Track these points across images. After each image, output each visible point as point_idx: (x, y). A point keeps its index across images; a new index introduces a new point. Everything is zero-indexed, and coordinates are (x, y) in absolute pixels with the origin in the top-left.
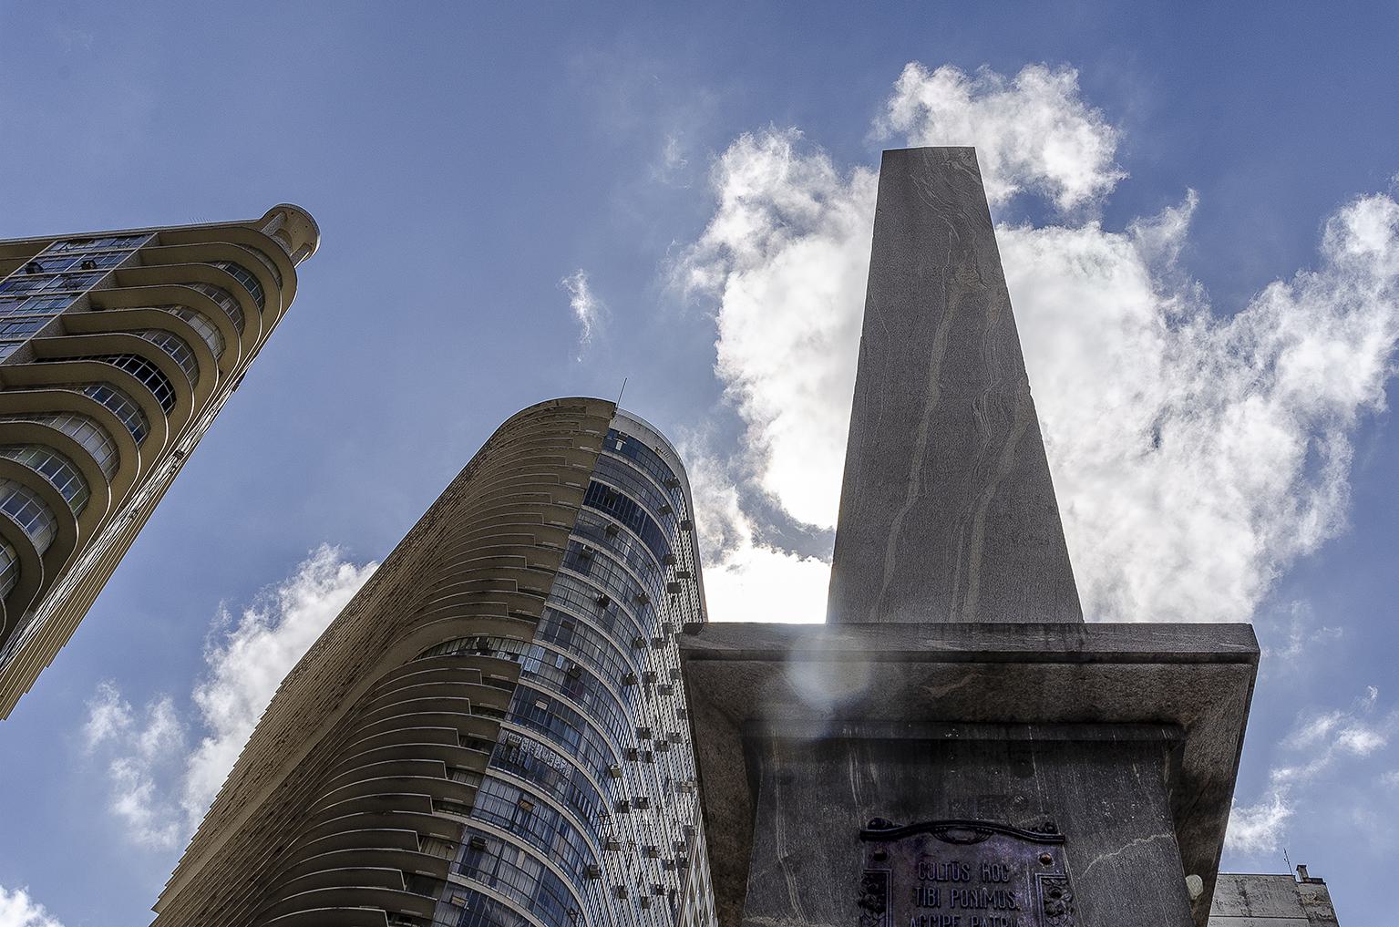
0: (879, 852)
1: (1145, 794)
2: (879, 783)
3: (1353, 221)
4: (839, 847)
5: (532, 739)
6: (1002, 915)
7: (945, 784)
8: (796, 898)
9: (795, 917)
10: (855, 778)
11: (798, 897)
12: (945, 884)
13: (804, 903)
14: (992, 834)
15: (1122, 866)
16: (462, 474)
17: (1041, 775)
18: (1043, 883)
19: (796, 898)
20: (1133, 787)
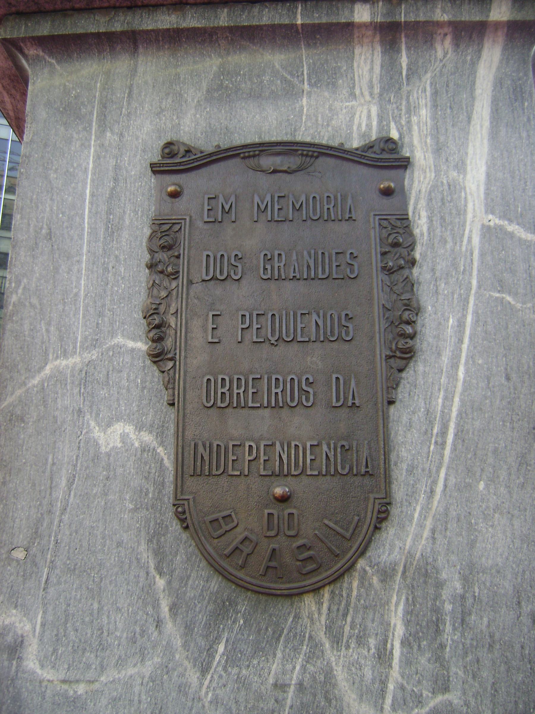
14: (317, 157)
18: (380, 224)
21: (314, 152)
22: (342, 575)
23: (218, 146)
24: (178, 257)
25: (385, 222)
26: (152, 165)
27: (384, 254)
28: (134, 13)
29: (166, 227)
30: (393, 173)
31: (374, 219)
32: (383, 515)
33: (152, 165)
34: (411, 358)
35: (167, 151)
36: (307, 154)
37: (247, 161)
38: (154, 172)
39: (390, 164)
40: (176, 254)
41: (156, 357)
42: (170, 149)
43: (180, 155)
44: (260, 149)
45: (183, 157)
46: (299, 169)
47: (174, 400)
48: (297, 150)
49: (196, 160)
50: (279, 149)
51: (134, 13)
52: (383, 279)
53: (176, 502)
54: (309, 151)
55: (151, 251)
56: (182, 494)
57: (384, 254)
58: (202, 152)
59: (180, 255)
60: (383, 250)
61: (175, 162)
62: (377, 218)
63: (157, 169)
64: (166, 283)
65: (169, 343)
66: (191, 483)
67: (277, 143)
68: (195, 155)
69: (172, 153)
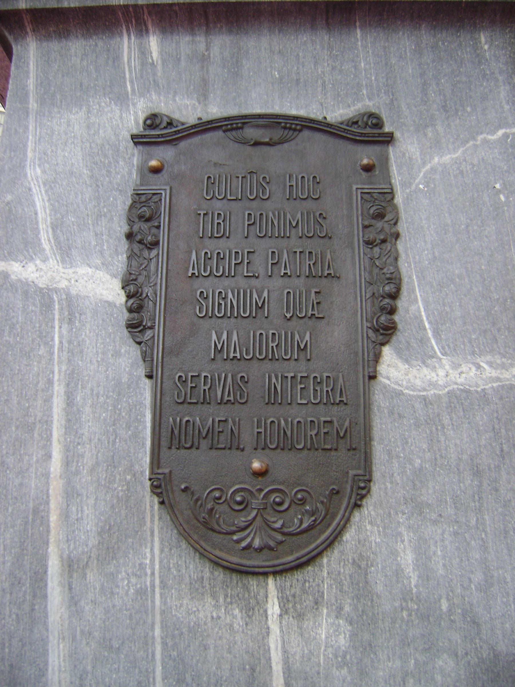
0: (154, 163)
1: (493, 73)
2: (160, 62)
3: (101, 295)
4: (106, 156)
5: (66, 59)
6: (309, 245)
7: (244, 62)
8: (47, 232)
9: (45, 260)
10: (129, 59)
11: (50, 230)
12: (239, 204)
13: (56, 237)
14: (300, 131)
15: (461, 172)
16: (389, 195)
17: (366, 47)
18: (362, 198)
19: (47, 232)
20: (480, 63)
21: (297, 125)
22: (320, 554)
23: (200, 119)
24: (158, 227)
25: (367, 195)
26: (133, 137)
27: (365, 227)
28: (349, 30)
29: (143, 198)
30: (377, 148)
31: (356, 191)
32: (364, 492)
33: (133, 137)
34: (392, 334)
35: (149, 122)
36: (288, 127)
37: (229, 134)
38: (136, 144)
39: (354, 137)
40: (156, 224)
41: (133, 328)
42: (153, 121)
43: (162, 126)
44: (243, 121)
45: (165, 128)
46: (281, 142)
47: (152, 372)
48: (280, 123)
49: (179, 132)
50: (261, 122)
51: (349, 30)
52: (366, 252)
53: (154, 476)
54: (292, 124)
55: (130, 222)
56: (158, 468)
57: (365, 227)
58: (183, 124)
59: (160, 226)
60: (366, 223)
61: (157, 132)
62: (359, 191)
63: (138, 140)
64: (146, 253)
65: (145, 315)
66: (170, 456)
67: (242, 116)
68: (177, 127)
69: (155, 125)
